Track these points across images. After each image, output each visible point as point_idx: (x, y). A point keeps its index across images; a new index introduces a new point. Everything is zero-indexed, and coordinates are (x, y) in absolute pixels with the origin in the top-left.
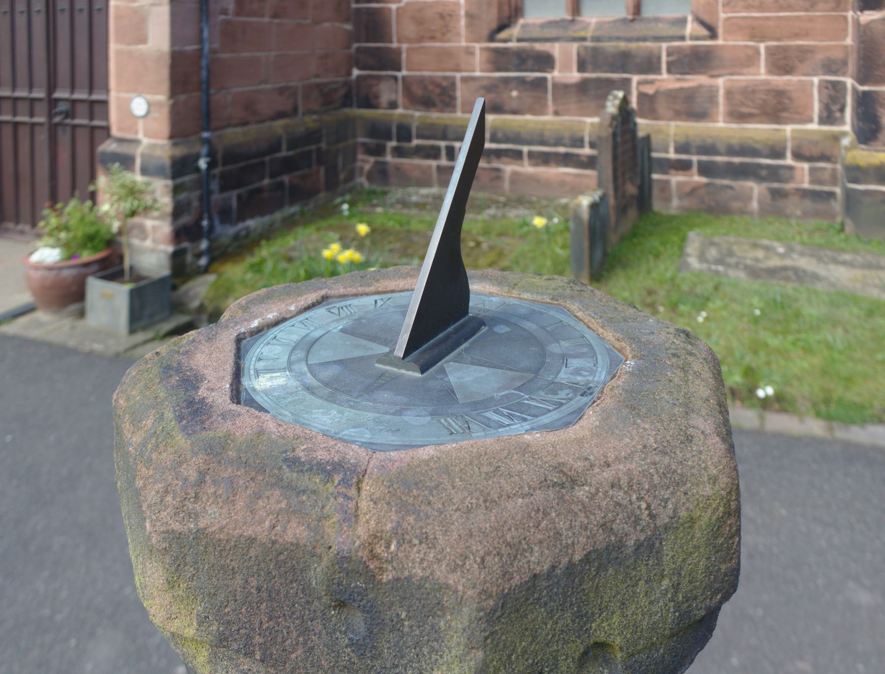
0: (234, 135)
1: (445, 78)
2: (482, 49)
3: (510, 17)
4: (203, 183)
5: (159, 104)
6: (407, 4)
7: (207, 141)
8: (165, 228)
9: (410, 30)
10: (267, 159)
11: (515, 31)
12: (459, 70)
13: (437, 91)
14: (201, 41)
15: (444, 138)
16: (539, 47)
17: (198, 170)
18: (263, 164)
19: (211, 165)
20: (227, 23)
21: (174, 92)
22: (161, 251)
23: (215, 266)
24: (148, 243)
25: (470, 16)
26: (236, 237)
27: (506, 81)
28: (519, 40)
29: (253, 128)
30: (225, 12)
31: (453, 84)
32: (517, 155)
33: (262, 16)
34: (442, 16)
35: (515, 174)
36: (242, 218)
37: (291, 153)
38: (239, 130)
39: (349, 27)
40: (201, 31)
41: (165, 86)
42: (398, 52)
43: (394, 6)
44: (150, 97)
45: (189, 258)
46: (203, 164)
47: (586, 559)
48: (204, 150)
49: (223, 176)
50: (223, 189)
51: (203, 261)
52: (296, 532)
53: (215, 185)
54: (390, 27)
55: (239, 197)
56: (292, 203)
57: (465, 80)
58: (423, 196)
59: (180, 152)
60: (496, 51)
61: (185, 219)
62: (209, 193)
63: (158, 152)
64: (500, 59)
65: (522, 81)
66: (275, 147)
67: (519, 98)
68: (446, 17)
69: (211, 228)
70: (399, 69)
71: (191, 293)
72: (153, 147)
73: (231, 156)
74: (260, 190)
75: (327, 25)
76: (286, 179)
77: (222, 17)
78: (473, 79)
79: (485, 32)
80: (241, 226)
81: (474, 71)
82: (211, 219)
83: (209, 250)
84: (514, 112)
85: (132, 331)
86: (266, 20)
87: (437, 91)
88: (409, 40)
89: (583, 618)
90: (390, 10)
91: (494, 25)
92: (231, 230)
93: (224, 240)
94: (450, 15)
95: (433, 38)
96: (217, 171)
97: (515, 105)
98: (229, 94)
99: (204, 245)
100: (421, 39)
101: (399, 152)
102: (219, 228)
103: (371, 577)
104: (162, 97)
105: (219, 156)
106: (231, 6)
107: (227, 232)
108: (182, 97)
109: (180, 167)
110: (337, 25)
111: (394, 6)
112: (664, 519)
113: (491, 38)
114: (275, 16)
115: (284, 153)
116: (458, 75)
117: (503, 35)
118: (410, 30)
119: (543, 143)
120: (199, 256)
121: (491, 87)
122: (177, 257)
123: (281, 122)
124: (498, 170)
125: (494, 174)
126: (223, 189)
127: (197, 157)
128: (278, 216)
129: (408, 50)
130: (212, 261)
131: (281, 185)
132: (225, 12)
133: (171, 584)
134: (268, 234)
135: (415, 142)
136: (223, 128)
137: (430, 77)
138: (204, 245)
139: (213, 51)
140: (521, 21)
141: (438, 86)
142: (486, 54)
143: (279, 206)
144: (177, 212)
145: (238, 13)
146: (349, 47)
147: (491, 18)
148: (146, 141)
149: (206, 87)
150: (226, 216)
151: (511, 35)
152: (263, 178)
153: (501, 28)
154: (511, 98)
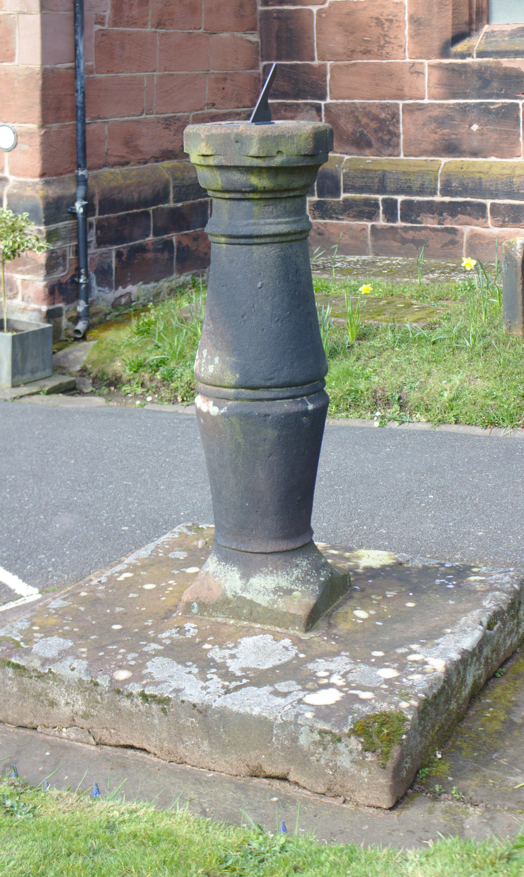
0: (111, 177)
1: (384, 107)
2: (430, 66)
3: (470, 23)
4: (79, 233)
5: (30, 134)
6: (332, 4)
7: (84, 181)
8: (38, 283)
9: (337, 41)
10: (151, 209)
11: (476, 42)
12: (401, 98)
13: (373, 125)
14: (76, 57)
15: (382, 190)
16: (506, 62)
17: (74, 215)
18: (147, 214)
19: (88, 210)
20: (103, 34)
21: (45, 122)
22: (34, 310)
23: (94, 332)
24: (18, 302)
25: (415, 21)
26: (115, 305)
27: (464, 109)
28: (480, 54)
29: (133, 169)
30: (100, 21)
31: (395, 116)
32: (479, 210)
33: (145, 25)
34: (379, 22)
35: (474, 236)
36: (121, 282)
37: (180, 205)
38: (117, 170)
39: (255, 38)
40: (76, 45)
41: (36, 112)
42: (321, 72)
43: (315, 9)
44: (16, 126)
45: (64, 322)
46: (79, 207)
47: (278, 136)
48: (81, 192)
49: (100, 226)
50: (100, 243)
51: (81, 326)
52: (229, 131)
53: (92, 237)
54: (311, 38)
55: (119, 255)
56: (181, 272)
57: (408, 109)
58: (349, 262)
59: (54, 192)
60: (451, 69)
61: (59, 274)
62: (87, 244)
63: (29, 192)
64: (456, 81)
65: (485, 110)
66: (161, 196)
67: (480, 132)
68: (384, 23)
69: (88, 287)
70: (323, 97)
71: (71, 357)
72: (22, 185)
73: (109, 204)
74: (142, 249)
75: (225, 35)
76: (174, 237)
77: (99, 27)
78: (421, 108)
79: (436, 44)
80: (121, 291)
81: (423, 99)
82: (87, 275)
83: (87, 314)
84: (475, 154)
85: (14, 385)
86: (149, 29)
87: (373, 125)
88: (335, 56)
89: (277, 145)
90: (311, 12)
91: (448, 34)
92: (111, 295)
93: (103, 306)
94: (391, 21)
95: (366, 53)
96: (92, 219)
97: (475, 144)
98: (107, 124)
99: (81, 307)
100: (351, 54)
101: (321, 209)
102: (96, 290)
103: (241, 136)
104: (33, 126)
105: (96, 202)
106: (108, 14)
107: (105, 296)
108: (55, 126)
109: (55, 211)
110: (239, 35)
111: (315, 9)
112: (294, 133)
113: (445, 52)
114: (159, 25)
115: (171, 204)
116: (401, 103)
117: (460, 47)
118: (337, 41)
119: (511, 195)
120: (75, 320)
121: (443, 120)
122: (51, 315)
123: (167, 164)
124: (453, 231)
125: (450, 237)
126: (100, 243)
127: (74, 199)
128: (164, 284)
129: (333, 68)
130: (90, 327)
131: (168, 244)
132: (100, 21)
133: (207, 145)
134: (157, 298)
135: (343, 196)
136: (99, 167)
137: (364, 107)
138: (81, 307)
139: (89, 71)
140: (486, 28)
141: (375, 118)
142: (436, 74)
143: (168, 273)
144: (52, 264)
145: (115, 24)
146: (255, 66)
147: (443, 24)
148: (12, 179)
149: (80, 114)
150: (104, 275)
151: (471, 47)
152: (147, 236)
153: (457, 38)
154: (470, 133)
